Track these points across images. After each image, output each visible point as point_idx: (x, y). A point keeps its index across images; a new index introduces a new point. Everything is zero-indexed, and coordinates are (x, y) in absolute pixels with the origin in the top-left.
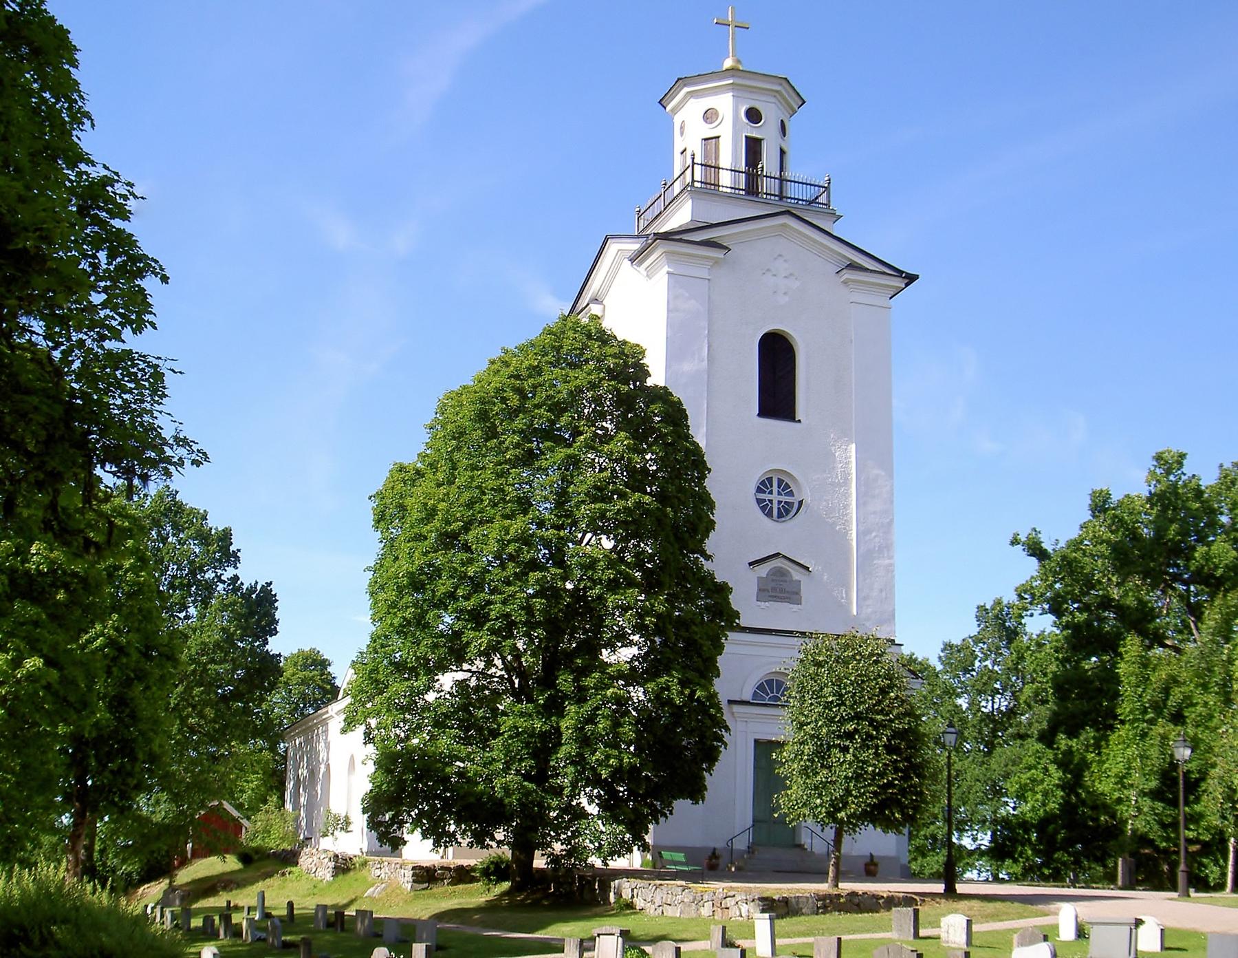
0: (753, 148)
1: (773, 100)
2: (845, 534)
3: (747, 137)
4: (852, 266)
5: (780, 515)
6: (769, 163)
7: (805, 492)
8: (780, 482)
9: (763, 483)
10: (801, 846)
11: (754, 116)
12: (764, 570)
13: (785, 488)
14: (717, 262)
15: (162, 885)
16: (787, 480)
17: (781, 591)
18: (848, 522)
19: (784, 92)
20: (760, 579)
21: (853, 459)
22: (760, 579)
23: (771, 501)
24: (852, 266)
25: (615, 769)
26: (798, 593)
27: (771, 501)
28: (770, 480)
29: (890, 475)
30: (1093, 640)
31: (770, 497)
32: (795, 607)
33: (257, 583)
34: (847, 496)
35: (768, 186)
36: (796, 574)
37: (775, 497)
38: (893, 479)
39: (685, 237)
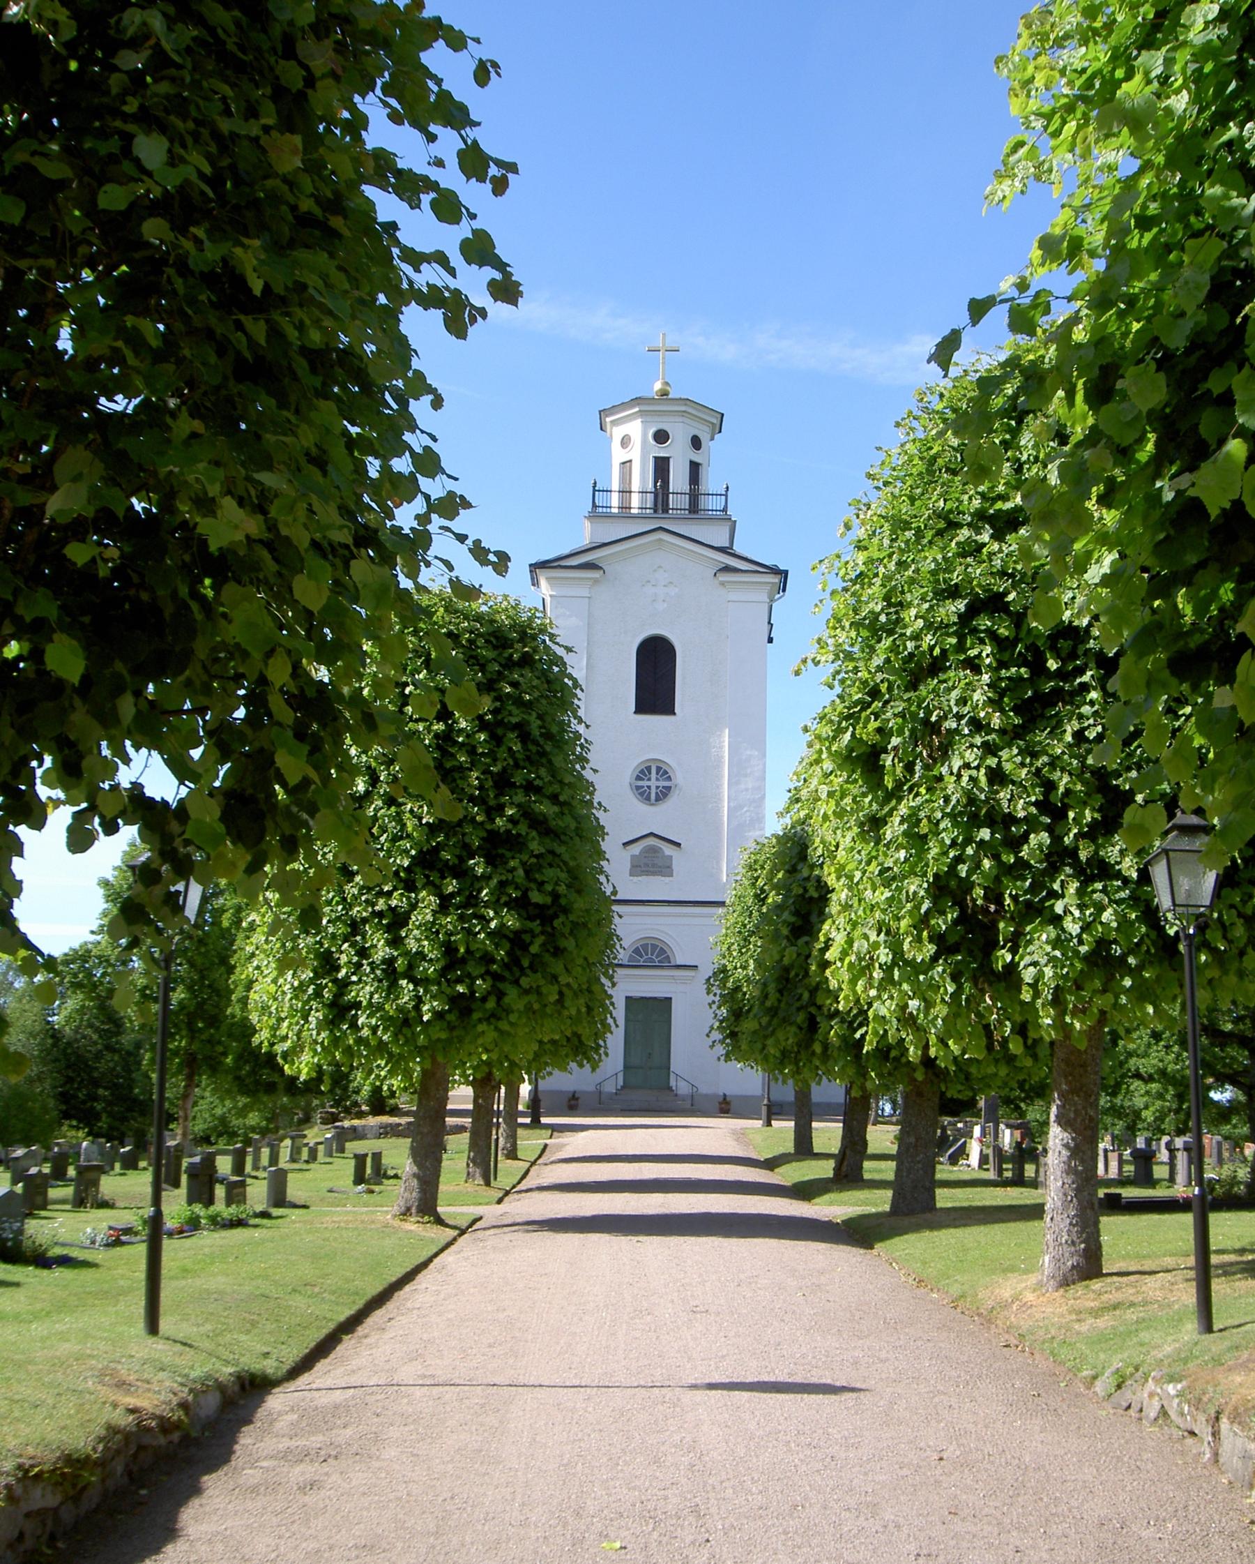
0: (662, 467)
1: (680, 419)
2: (718, 810)
3: (656, 458)
4: (727, 569)
5: (658, 799)
6: (678, 480)
7: (679, 777)
8: (659, 769)
9: (642, 772)
10: (670, 1089)
11: (661, 437)
12: (636, 849)
13: (663, 773)
14: (596, 581)
15: (64, 1234)
16: (664, 767)
17: (654, 865)
18: (720, 800)
19: (690, 410)
20: (632, 856)
21: (726, 744)
22: (632, 856)
23: (649, 787)
24: (727, 569)
25: (424, 868)
26: (670, 867)
27: (649, 787)
28: (649, 769)
29: (763, 755)
30: (1131, 960)
31: (648, 783)
32: (667, 879)
33: (499, 75)
34: (720, 777)
35: (678, 501)
36: (668, 850)
37: (653, 783)
38: (764, 756)
39: (563, 563)
